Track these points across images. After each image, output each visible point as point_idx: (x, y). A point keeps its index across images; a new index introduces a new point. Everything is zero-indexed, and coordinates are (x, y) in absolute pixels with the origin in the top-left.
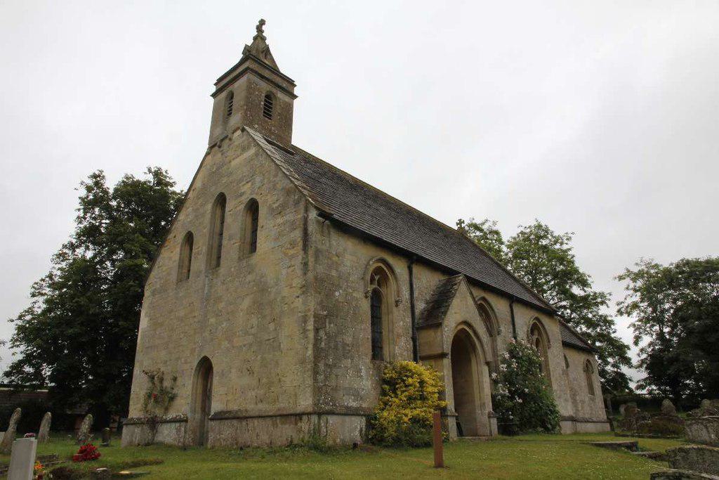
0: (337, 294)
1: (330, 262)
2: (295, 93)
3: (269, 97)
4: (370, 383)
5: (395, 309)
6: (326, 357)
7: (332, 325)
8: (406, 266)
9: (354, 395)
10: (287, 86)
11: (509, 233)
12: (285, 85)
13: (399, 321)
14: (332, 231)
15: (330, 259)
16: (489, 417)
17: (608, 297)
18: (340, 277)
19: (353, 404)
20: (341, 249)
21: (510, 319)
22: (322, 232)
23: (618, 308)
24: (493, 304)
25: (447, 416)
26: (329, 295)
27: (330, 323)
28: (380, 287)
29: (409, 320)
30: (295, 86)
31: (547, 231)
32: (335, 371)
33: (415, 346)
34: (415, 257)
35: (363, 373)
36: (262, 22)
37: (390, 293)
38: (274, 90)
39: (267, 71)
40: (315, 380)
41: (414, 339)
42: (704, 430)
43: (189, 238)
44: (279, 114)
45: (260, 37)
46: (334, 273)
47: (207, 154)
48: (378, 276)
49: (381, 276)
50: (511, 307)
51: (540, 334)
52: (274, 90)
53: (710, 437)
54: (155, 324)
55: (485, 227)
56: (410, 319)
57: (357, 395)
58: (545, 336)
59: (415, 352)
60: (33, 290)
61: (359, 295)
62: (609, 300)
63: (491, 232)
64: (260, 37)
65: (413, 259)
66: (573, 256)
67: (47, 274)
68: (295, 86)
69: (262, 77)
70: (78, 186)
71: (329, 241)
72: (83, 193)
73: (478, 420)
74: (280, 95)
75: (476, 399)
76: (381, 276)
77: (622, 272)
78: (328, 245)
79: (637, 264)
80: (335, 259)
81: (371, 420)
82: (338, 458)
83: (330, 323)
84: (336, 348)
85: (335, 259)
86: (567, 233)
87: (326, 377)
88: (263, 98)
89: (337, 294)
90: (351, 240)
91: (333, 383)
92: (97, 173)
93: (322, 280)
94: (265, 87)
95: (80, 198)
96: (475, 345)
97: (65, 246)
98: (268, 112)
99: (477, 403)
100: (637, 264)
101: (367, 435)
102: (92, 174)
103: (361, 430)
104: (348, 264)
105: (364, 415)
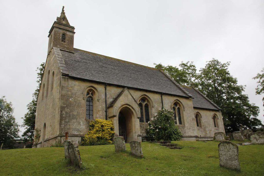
0: (71, 99)
1: (68, 90)
2: (75, 32)
3: (64, 35)
4: (84, 126)
5: (97, 102)
6: (65, 119)
7: (68, 109)
8: (104, 87)
9: (77, 131)
10: (72, 30)
11: (200, 65)
12: (70, 29)
13: (99, 106)
14: (69, 79)
15: (68, 89)
16: (138, 136)
17: (244, 87)
18: (72, 94)
19: (76, 133)
20: (73, 85)
21: (161, 101)
22: (65, 80)
23: (256, 91)
24: (149, 97)
25: (114, 136)
26: (67, 100)
27: (67, 109)
28: (93, 96)
29: (104, 105)
30: (75, 29)
31: (218, 62)
32: (68, 123)
33: (106, 114)
34: (106, 84)
35: (81, 123)
36: (63, 7)
37: (96, 97)
38: (65, 32)
39: (62, 26)
40: (60, 126)
41: (106, 112)
42: (221, 136)
43: (44, 84)
44: (68, 40)
45: (63, 13)
46: (69, 93)
47: (47, 57)
48: (91, 92)
49: (91, 93)
50: (161, 97)
51: (180, 105)
52: (65, 32)
53: (223, 139)
54: (38, 114)
55: (188, 65)
56: (105, 105)
57: (78, 130)
58: (182, 106)
59: (106, 116)
60: (28, 107)
61: (81, 99)
62: (245, 88)
63: (191, 66)
64: (63, 13)
65: (106, 85)
66: (228, 71)
67: (32, 101)
68: (75, 29)
69: (60, 28)
70: (37, 69)
71: (68, 83)
72: (39, 72)
73: (134, 137)
74: (68, 33)
75: (133, 130)
76: (91, 93)
77: (256, 75)
78: (67, 84)
79: (262, 71)
80: (71, 88)
81: (83, 138)
82: (236, 172)
83: (67, 109)
84: (70, 116)
85: (71, 88)
86: (228, 62)
87: (65, 126)
88: (61, 35)
89: (71, 99)
90: (78, 81)
91: (68, 127)
92: (43, 64)
93: (64, 96)
94: (61, 32)
95: (38, 73)
96: (133, 112)
97: (36, 91)
98: (64, 39)
99: (134, 132)
100: (262, 71)
101: (81, 143)
102: (41, 64)
103: (79, 142)
104: (76, 89)
105: (81, 137)
